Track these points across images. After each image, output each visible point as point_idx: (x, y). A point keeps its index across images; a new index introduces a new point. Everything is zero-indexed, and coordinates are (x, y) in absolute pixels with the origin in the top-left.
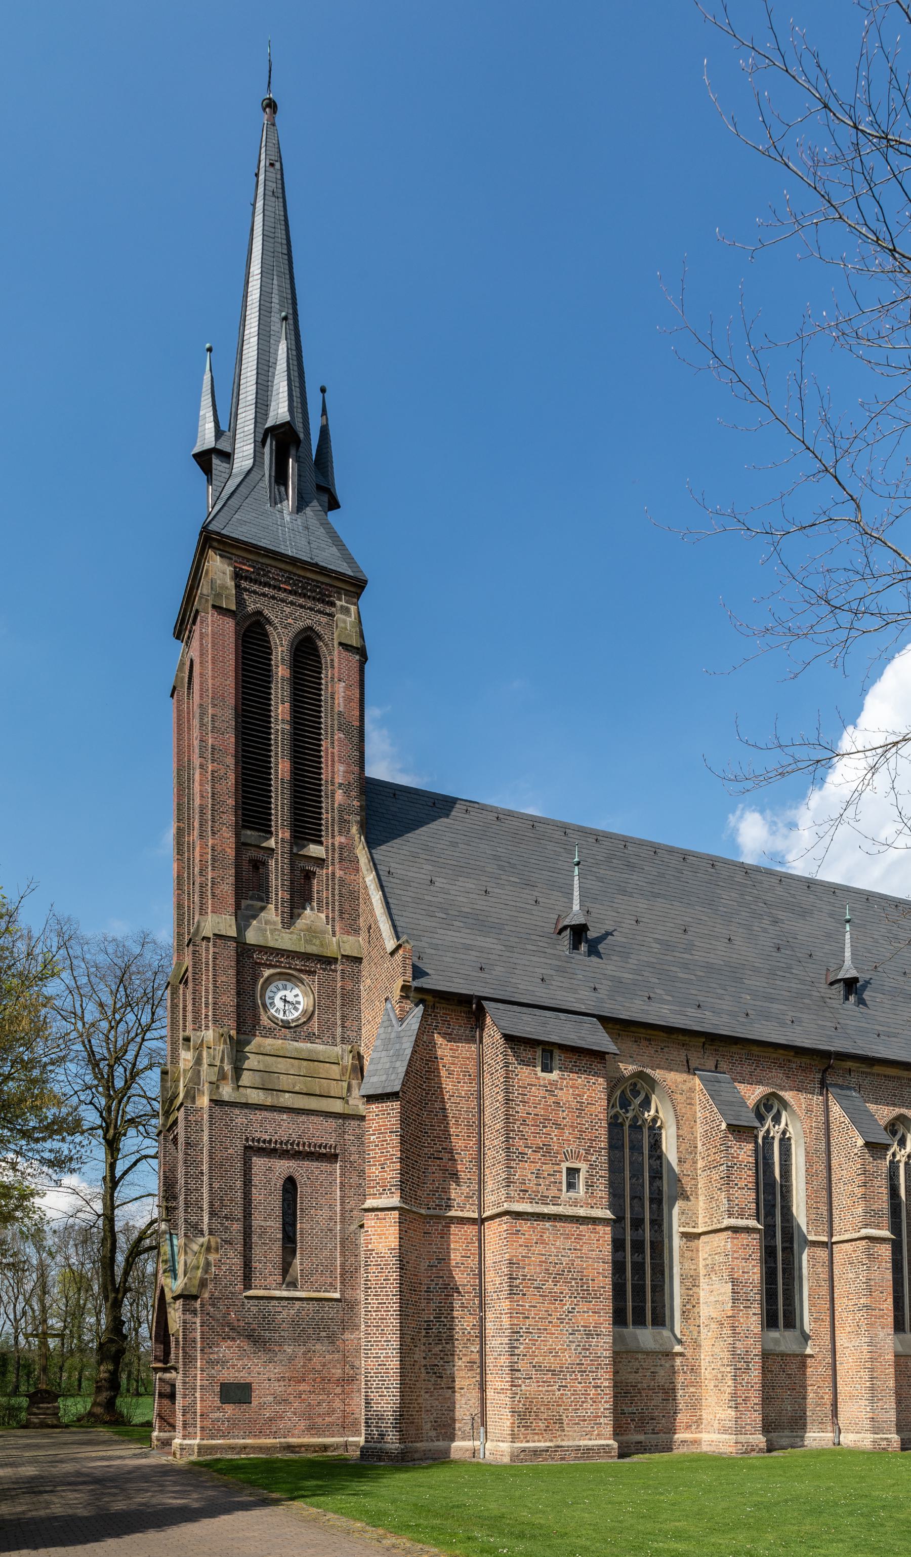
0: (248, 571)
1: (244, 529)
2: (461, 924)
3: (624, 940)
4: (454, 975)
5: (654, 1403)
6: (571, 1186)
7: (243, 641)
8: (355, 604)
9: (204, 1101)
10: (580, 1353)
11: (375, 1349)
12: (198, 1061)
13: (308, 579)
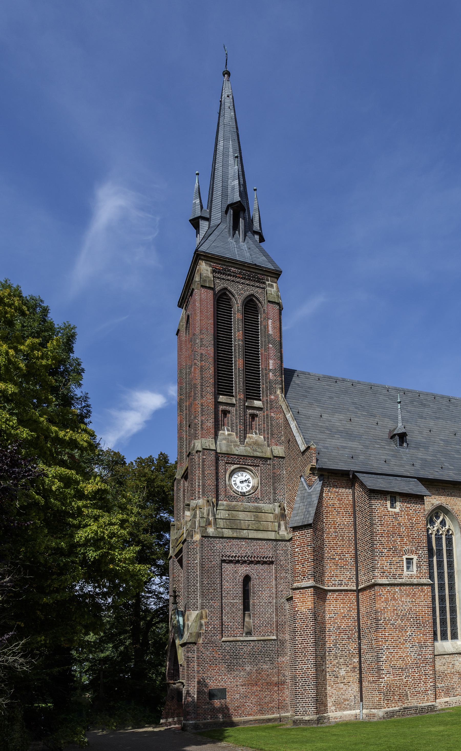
0: (219, 269)
1: (218, 250)
2: (339, 436)
3: (425, 440)
4: (338, 461)
5: (454, 680)
6: (408, 568)
7: (217, 302)
8: (276, 283)
9: (197, 537)
10: (416, 657)
11: (300, 665)
12: (195, 516)
13: (251, 272)
